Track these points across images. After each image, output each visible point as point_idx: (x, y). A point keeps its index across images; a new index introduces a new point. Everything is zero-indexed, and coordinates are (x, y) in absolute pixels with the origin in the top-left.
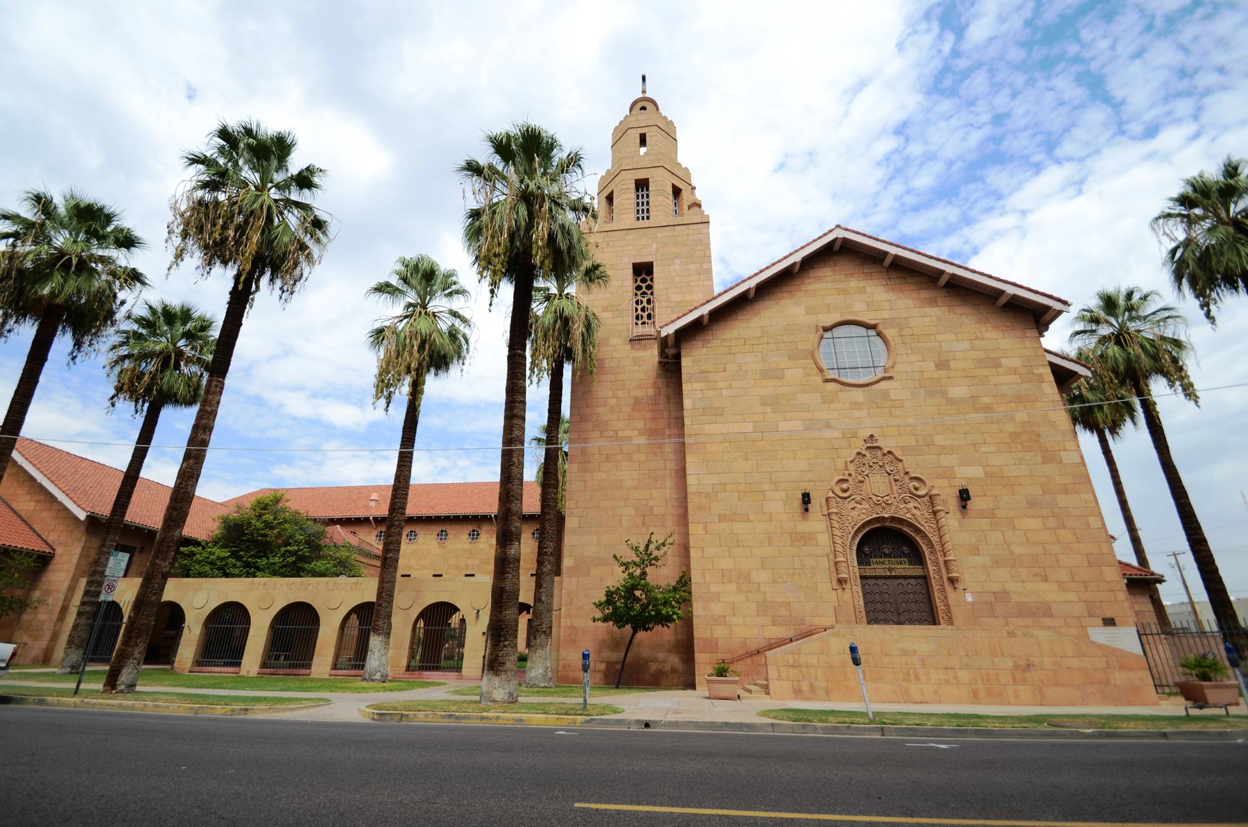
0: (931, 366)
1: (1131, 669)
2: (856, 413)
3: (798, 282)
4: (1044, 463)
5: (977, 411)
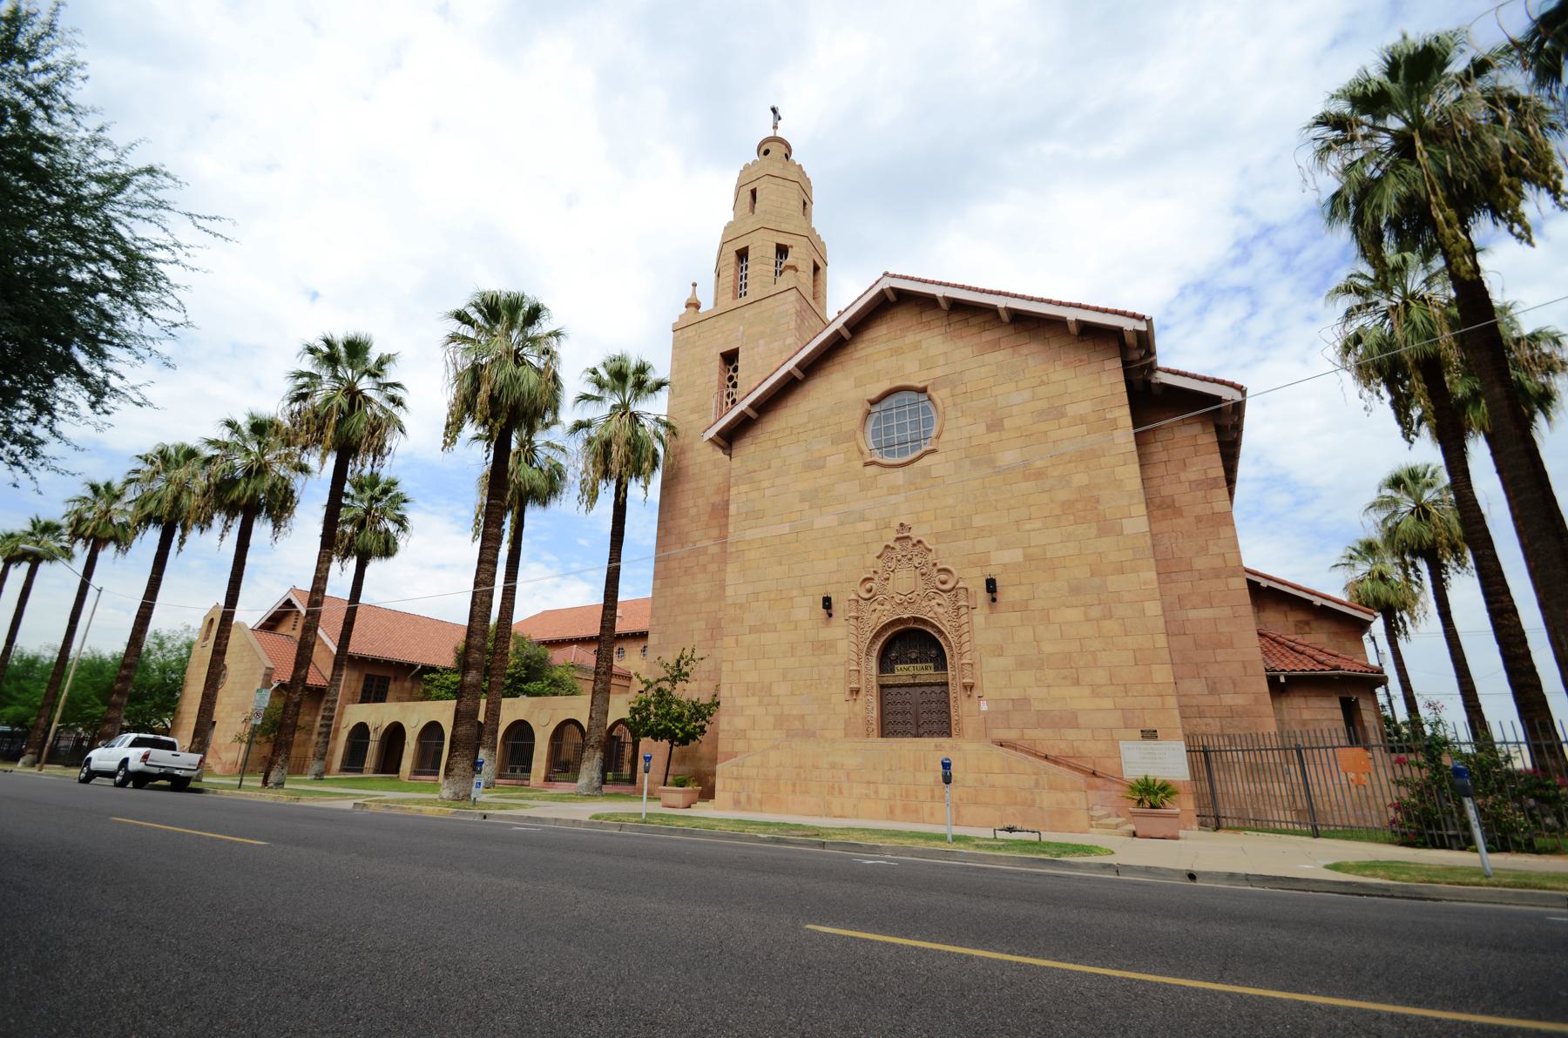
0: (982, 428)
1: (1063, 790)
3: (851, 349)
4: (1099, 536)
5: (1026, 478)
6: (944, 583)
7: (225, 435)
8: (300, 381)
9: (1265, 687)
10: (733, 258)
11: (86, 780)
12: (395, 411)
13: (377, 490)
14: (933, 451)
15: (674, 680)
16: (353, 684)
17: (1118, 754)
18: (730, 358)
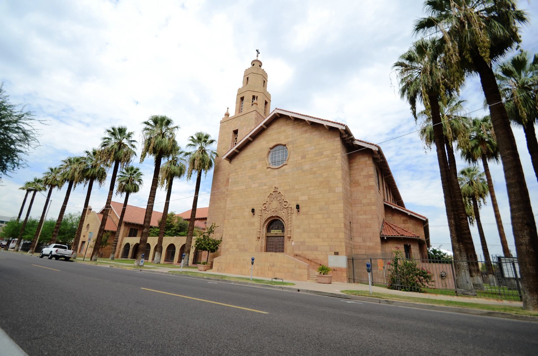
2: (274, 179)
3: (266, 131)
4: (329, 193)
6: (285, 205)
7: (85, 155)
8: (106, 140)
9: (379, 240)
10: (239, 100)
11: (42, 257)
12: (133, 149)
13: (133, 171)
14: (286, 164)
15: (209, 233)
16: (126, 231)
17: (327, 259)
18: (236, 132)
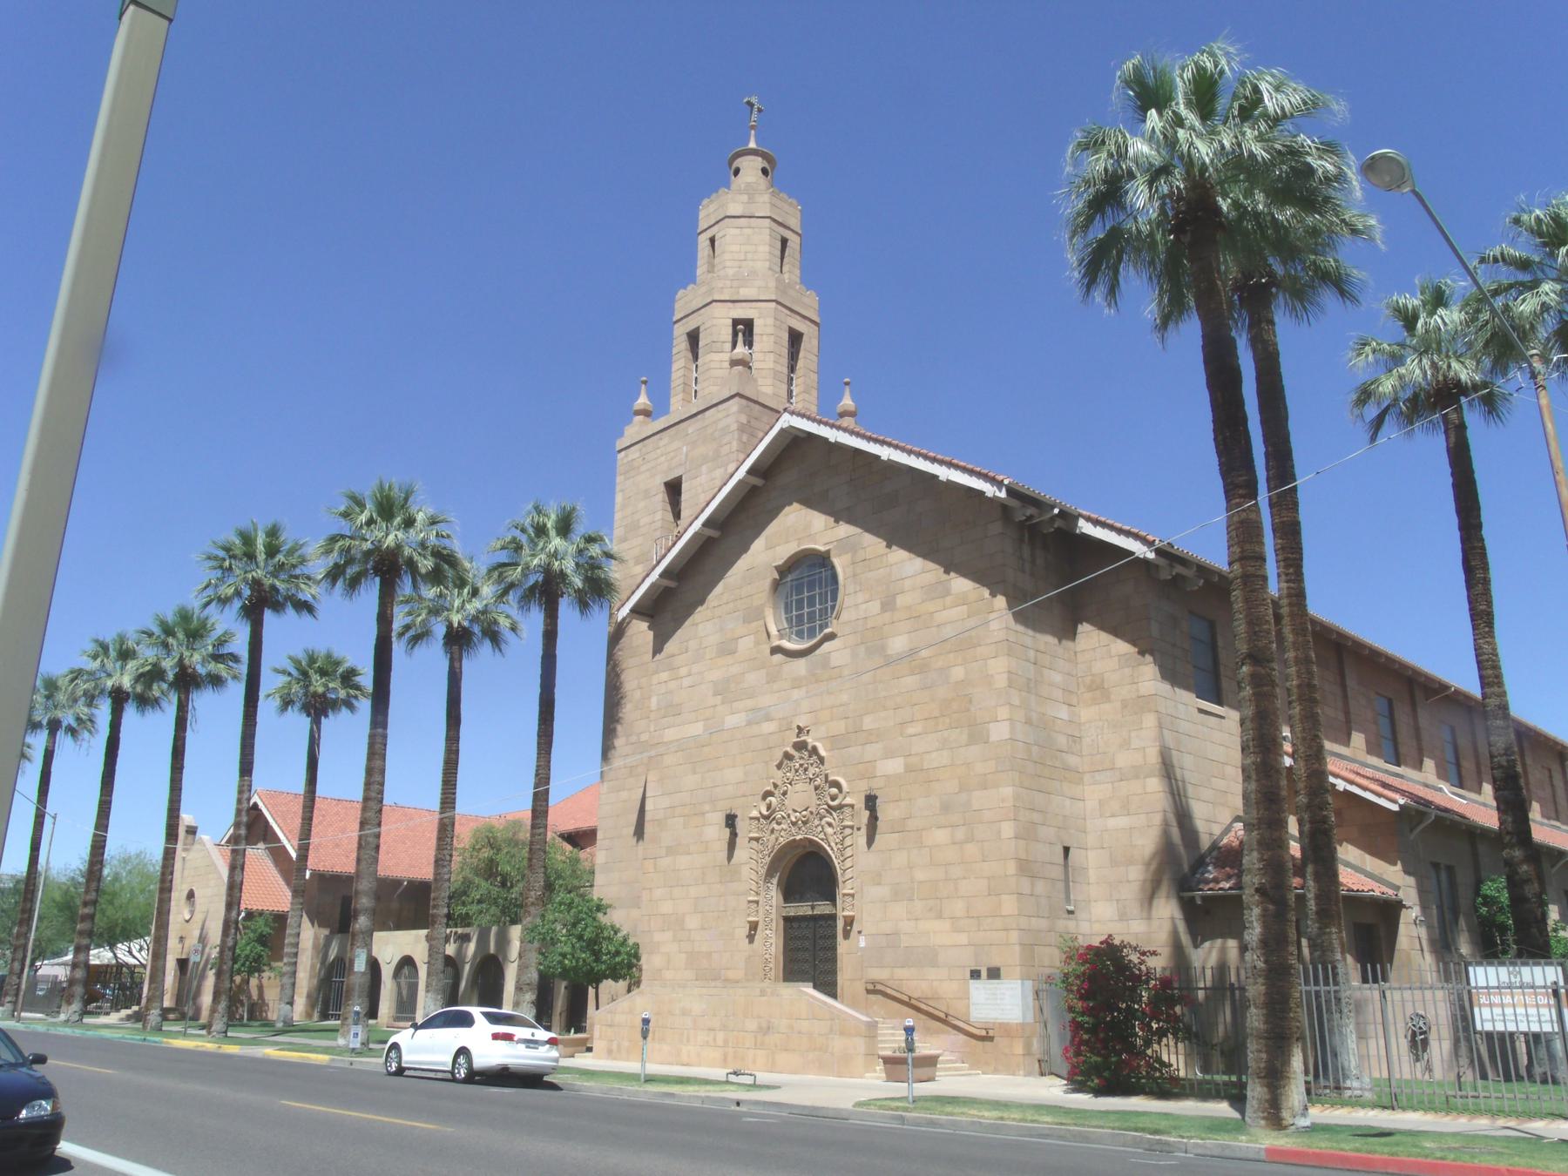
2: (796, 694)
18: (674, 489)
